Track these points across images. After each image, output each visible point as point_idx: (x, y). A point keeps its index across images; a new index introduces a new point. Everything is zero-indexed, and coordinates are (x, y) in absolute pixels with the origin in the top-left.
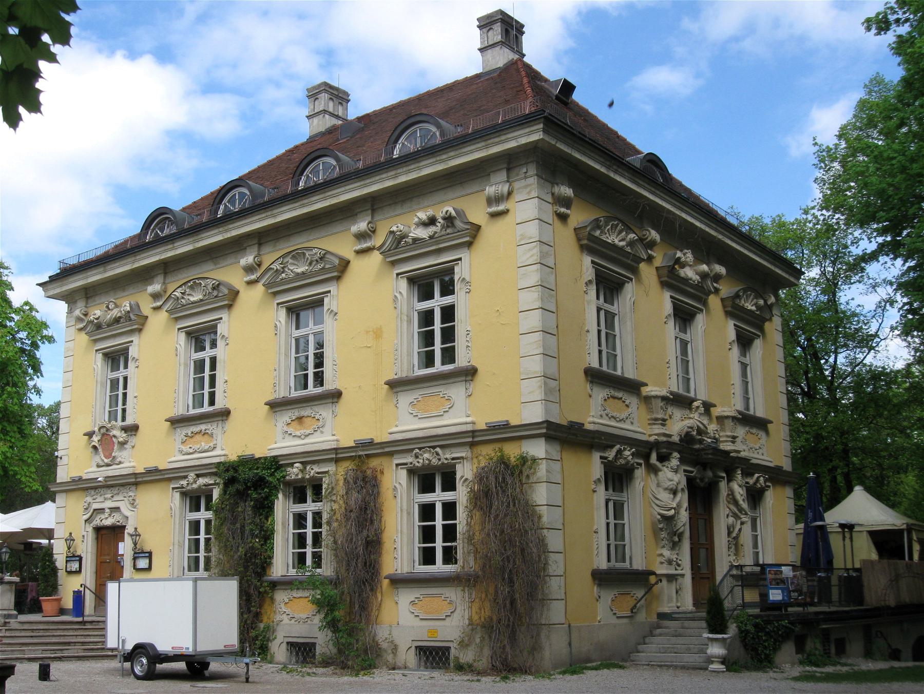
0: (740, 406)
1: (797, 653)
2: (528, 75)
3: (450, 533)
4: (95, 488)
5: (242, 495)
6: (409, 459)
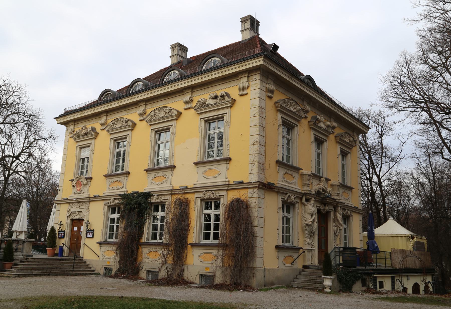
0: (341, 181)
1: (362, 286)
2: (259, 41)
3: (217, 227)
4: (73, 203)
5: (132, 210)
6: (201, 195)
